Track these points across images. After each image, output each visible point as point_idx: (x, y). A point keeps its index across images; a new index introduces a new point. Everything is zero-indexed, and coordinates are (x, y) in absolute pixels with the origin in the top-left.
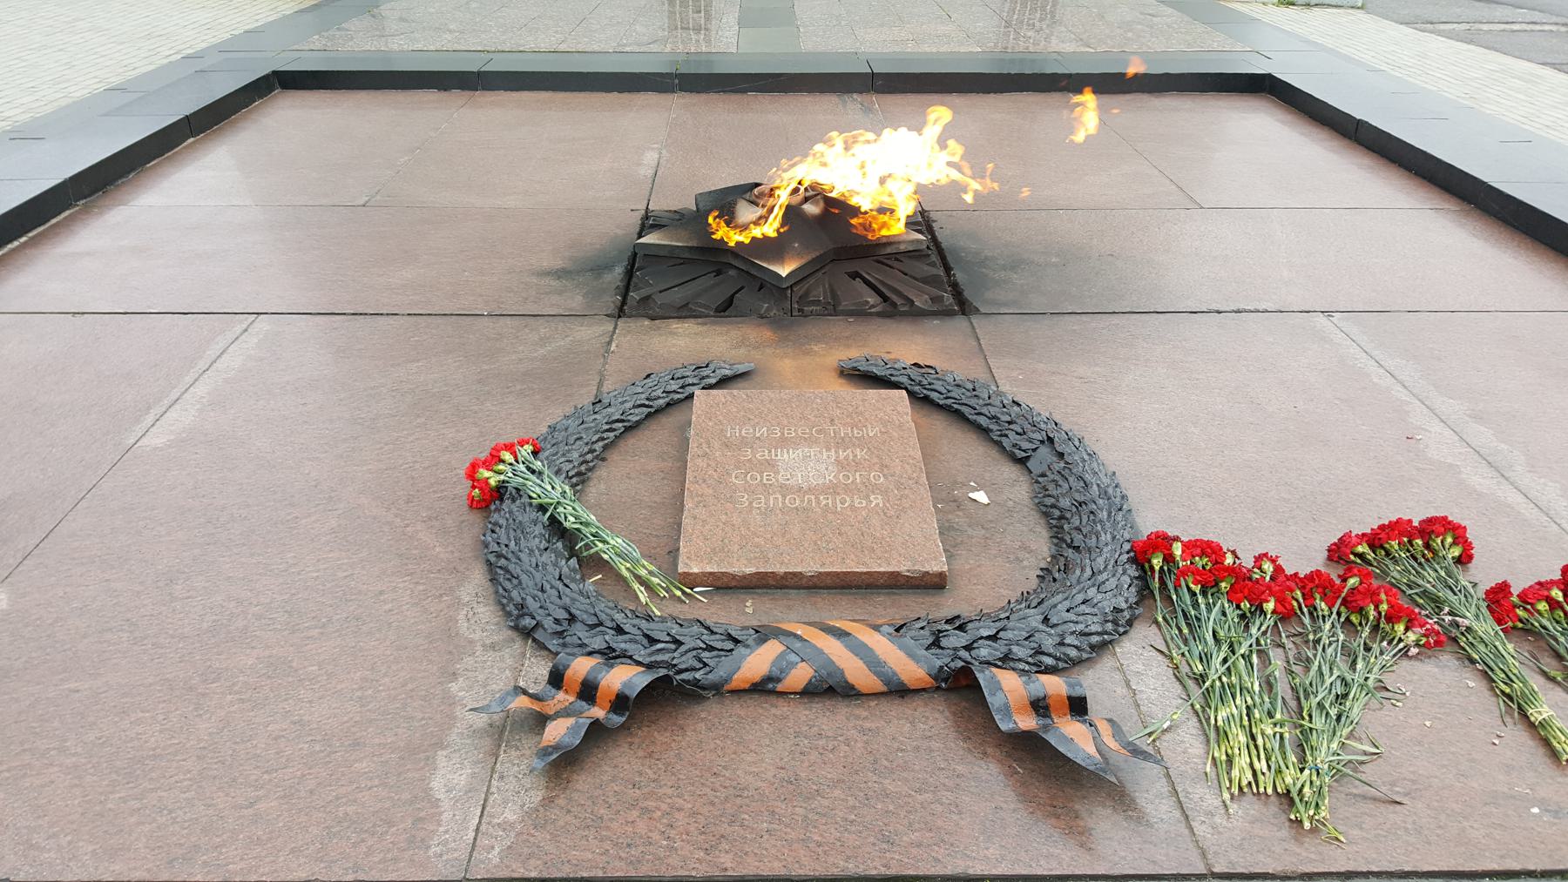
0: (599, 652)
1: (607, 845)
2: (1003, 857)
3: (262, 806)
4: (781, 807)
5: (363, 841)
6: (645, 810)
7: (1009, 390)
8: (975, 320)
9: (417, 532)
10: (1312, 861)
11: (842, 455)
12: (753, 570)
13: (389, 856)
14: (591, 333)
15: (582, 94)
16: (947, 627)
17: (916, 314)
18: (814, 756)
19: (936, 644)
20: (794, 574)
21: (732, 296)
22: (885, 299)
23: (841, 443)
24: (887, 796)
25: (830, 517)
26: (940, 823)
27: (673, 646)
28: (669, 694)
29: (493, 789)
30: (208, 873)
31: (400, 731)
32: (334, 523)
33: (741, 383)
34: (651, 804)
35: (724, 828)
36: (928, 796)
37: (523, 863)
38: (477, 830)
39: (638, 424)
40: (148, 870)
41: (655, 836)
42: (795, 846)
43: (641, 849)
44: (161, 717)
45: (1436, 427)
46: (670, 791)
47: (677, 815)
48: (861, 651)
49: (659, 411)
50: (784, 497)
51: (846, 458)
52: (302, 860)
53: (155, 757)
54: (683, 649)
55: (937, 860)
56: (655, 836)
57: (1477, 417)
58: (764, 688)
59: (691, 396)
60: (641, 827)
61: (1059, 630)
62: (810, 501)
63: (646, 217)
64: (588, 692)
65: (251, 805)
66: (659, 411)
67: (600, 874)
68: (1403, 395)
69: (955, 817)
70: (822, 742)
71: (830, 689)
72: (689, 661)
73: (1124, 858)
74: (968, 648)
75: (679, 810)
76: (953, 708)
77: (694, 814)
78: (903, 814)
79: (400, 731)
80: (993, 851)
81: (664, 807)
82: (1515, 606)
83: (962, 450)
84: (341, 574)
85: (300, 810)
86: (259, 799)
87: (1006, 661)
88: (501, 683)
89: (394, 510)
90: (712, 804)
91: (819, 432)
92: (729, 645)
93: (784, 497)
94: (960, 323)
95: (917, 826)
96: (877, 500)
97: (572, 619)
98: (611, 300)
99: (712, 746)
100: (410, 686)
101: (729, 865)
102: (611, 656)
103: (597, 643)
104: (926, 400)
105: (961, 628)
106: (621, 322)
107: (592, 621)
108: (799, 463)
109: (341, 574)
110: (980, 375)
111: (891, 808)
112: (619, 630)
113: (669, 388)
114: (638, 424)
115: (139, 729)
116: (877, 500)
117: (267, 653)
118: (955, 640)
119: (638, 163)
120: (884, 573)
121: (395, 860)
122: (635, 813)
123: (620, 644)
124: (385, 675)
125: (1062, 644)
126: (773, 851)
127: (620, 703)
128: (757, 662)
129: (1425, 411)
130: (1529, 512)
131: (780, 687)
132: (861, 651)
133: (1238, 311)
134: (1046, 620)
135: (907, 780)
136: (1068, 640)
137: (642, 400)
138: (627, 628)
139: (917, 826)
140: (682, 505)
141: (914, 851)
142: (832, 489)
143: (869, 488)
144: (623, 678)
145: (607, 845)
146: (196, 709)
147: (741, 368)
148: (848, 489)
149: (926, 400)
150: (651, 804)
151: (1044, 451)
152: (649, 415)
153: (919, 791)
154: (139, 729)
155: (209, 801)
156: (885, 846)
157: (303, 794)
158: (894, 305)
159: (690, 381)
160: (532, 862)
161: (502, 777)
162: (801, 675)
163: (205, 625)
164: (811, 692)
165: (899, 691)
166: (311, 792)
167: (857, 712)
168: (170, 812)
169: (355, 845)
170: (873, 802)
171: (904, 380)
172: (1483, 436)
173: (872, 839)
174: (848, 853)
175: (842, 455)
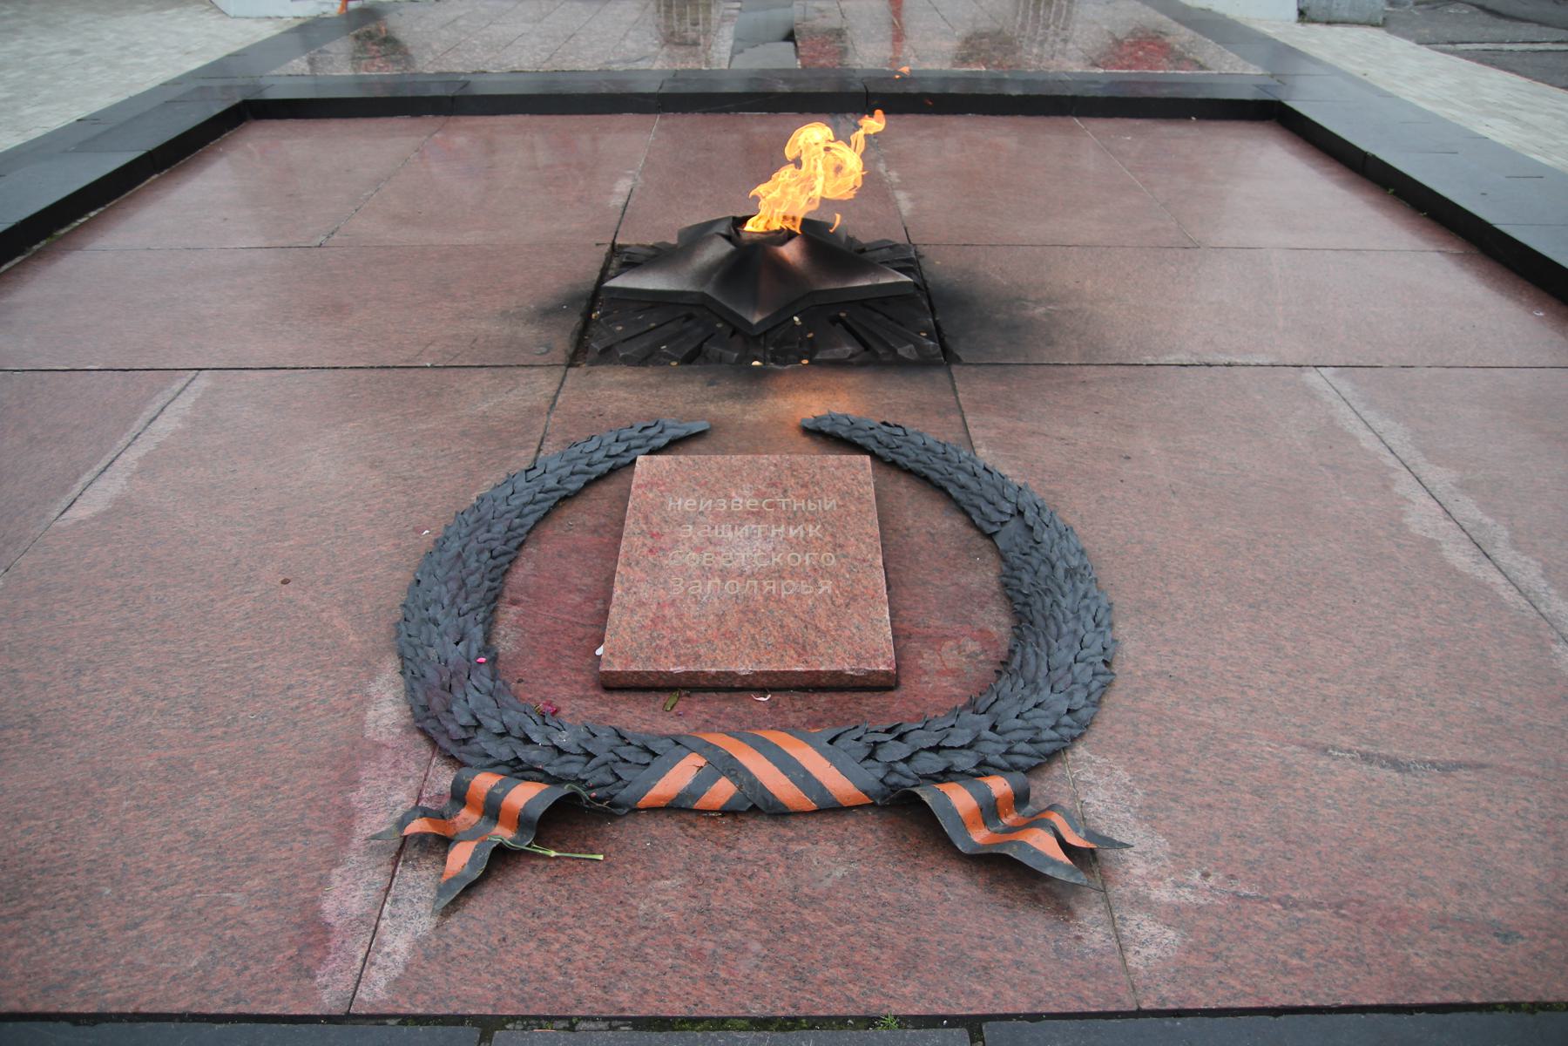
0: (506, 763)
1: (499, 980)
2: (921, 996)
3: (147, 927)
4: (690, 942)
5: (246, 968)
6: (543, 941)
7: (984, 454)
8: (955, 368)
9: (331, 618)
10: (1245, 995)
11: (792, 533)
12: (680, 669)
13: (273, 986)
14: (542, 384)
15: (589, 117)
16: (888, 737)
17: (902, 364)
18: (730, 882)
19: (871, 756)
20: (726, 673)
21: (701, 345)
22: (866, 347)
23: (793, 519)
24: (805, 928)
25: (772, 605)
26: (857, 958)
27: (583, 759)
28: (574, 817)
29: (385, 914)
30: (85, 1002)
31: (296, 845)
32: (248, 606)
33: (696, 445)
34: (550, 935)
35: (626, 964)
36: (849, 928)
37: (410, 998)
38: (365, 961)
39: (577, 493)
40: (22, 1000)
41: (552, 971)
42: (700, 984)
43: (536, 985)
44: (53, 826)
45: (1421, 498)
46: (570, 921)
47: (576, 947)
48: (787, 765)
49: (601, 478)
50: (723, 581)
51: (797, 537)
52: (182, 989)
53: (43, 871)
54: (594, 762)
55: (850, 999)
56: (552, 971)
57: (1465, 487)
58: (679, 808)
59: (634, 461)
60: (538, 960)
61: (1008, 737)
62: (752, 586)
63: (615, 250)
64: (492, 810)
65: (136, 925)
66: (601, 478)
67: (490, 1012)
68: (1390, 461)
69: (874, 951)
70: (740, 867)
71: (755, 808)
72: (603, 776)
73: (1049, 994)
74: (907, 760)
75: (579, 942)
76: (887, 827)
77: (593, 947)
78: (819, 948)
79: (296, 845)
80: (911, 988)
81: (564, 939)
82: (904, 186)
83: (929, 521)
84: (251, 665)
85: (187, 933)
86: (146, 918)
87: (947, 775)
88: (403, 798)
89: (311, 593)
90: (616, 936)
91: (770, 505)
92: (646, 758)
93: (723, 581)
94: (940, 376)
95: (833, 961)
96: (826, 586)
97: (479, 725)
98: (562, 343)
99: (621, 871)
100: (311, 795)
101: (626, 1005)
102: (519, 770)
103: (503, 751)
104: (893, 464)
105: (900, 738)
106: (573, 371)
107: (500, 729)
108: (742, 539)
109: (251, 665)
110: (951, 436)
111: (808, 941)
112: (527, 740)
113: (613, 452)
114: (577, 493)
115: (30, 838)
116: (826, 586)
117: (169, 753)
118: (894, 751)
119: (630, 184)
120: (825, 673)
121: (279, 991)
122: (532, 945)
123: (529, 754)
124: (286, 781)
125: (1009, 752)
126: (676, 990)
127: (522, 822)
128: (678, 777)
129: (1411, 479)
130: (1508, 595)
131: (698, 805)
132: (787, 765)
133: (1229, 365)
134: (993, 728)
135: (827, 910)
136: (1017, 748)
137: (581, 465)
138: (535, 738)
139: (833, 961)
140: (611, 594)
141: (827, 989)
142: (779, 574)
143: (818, 572)
144: (524, 795)
145: (499, 980)
146: (90, 817)
147: (698, 427)
148: (794, 573)
149: (893, 464)
150: (550, 935)
151: (1014, 524)
152: (588, 484)
153: (840, 922)
154: (30, 838)
155: (93, 921)
156: (796, 983)
157: (190, 914)
158: (876, 354)
159: (634, 443)
160: (420, 997)
161: (395, 901)
162: (723, 791)
163: (109, 722)
164: (729, 812)
165: (831, 809)
166: (200, 912)
167: (782, 831)
168: (53, 932)
169: (239, 973)
170: (788, 935)
171: (872, 444)
172: (1468, 509)
173: (782, 977)
174: (757, 992)
175: (792, 533)
